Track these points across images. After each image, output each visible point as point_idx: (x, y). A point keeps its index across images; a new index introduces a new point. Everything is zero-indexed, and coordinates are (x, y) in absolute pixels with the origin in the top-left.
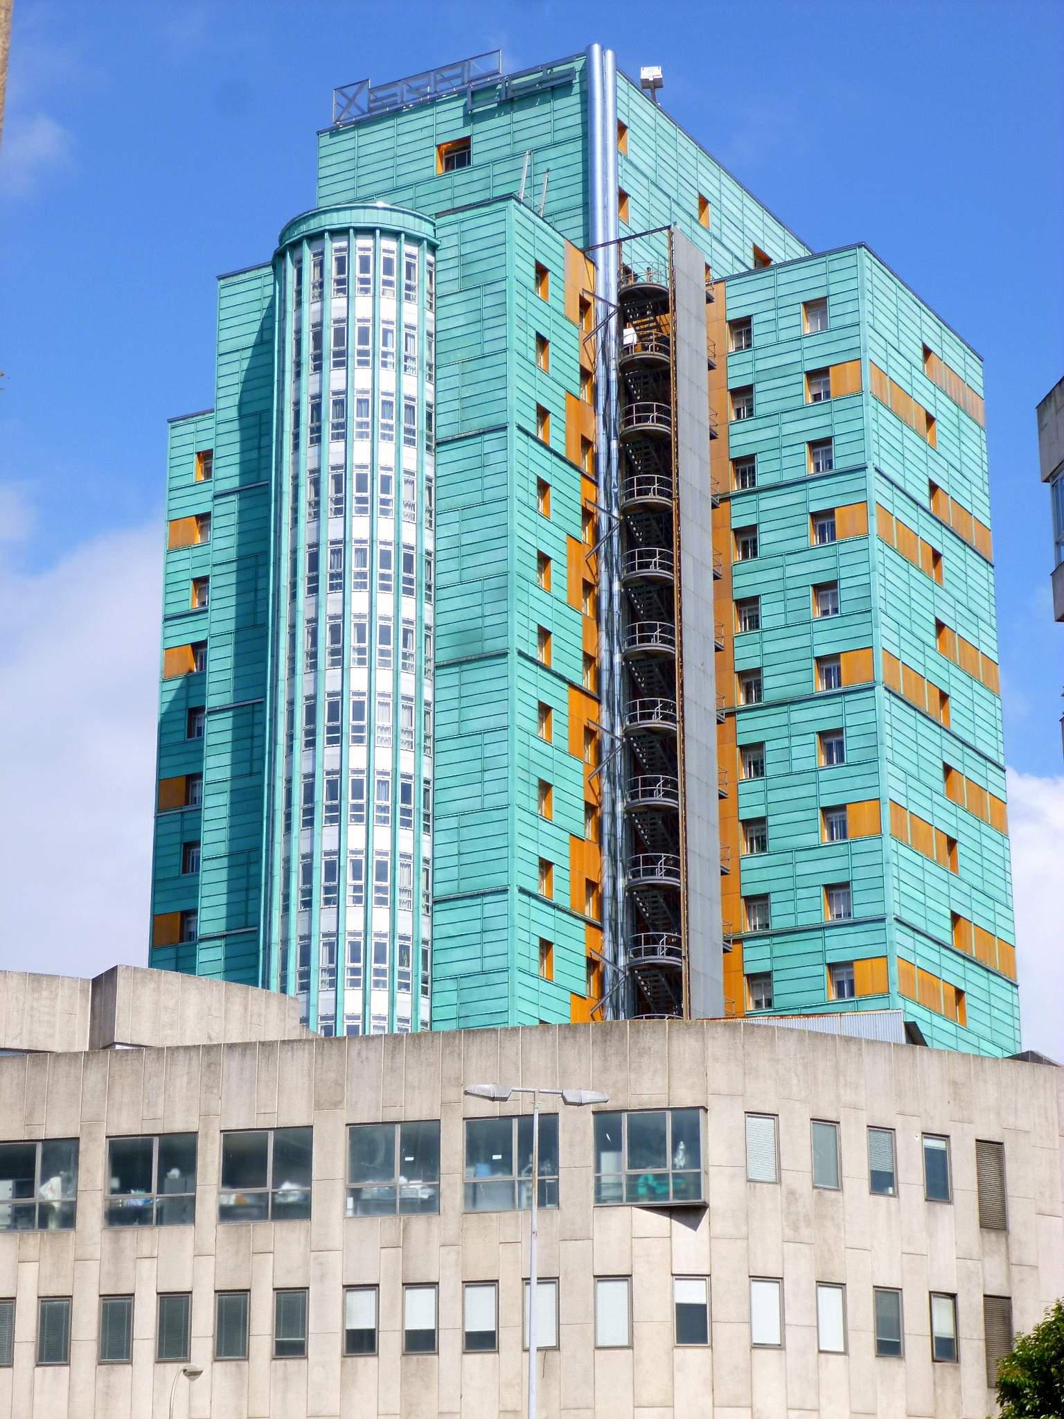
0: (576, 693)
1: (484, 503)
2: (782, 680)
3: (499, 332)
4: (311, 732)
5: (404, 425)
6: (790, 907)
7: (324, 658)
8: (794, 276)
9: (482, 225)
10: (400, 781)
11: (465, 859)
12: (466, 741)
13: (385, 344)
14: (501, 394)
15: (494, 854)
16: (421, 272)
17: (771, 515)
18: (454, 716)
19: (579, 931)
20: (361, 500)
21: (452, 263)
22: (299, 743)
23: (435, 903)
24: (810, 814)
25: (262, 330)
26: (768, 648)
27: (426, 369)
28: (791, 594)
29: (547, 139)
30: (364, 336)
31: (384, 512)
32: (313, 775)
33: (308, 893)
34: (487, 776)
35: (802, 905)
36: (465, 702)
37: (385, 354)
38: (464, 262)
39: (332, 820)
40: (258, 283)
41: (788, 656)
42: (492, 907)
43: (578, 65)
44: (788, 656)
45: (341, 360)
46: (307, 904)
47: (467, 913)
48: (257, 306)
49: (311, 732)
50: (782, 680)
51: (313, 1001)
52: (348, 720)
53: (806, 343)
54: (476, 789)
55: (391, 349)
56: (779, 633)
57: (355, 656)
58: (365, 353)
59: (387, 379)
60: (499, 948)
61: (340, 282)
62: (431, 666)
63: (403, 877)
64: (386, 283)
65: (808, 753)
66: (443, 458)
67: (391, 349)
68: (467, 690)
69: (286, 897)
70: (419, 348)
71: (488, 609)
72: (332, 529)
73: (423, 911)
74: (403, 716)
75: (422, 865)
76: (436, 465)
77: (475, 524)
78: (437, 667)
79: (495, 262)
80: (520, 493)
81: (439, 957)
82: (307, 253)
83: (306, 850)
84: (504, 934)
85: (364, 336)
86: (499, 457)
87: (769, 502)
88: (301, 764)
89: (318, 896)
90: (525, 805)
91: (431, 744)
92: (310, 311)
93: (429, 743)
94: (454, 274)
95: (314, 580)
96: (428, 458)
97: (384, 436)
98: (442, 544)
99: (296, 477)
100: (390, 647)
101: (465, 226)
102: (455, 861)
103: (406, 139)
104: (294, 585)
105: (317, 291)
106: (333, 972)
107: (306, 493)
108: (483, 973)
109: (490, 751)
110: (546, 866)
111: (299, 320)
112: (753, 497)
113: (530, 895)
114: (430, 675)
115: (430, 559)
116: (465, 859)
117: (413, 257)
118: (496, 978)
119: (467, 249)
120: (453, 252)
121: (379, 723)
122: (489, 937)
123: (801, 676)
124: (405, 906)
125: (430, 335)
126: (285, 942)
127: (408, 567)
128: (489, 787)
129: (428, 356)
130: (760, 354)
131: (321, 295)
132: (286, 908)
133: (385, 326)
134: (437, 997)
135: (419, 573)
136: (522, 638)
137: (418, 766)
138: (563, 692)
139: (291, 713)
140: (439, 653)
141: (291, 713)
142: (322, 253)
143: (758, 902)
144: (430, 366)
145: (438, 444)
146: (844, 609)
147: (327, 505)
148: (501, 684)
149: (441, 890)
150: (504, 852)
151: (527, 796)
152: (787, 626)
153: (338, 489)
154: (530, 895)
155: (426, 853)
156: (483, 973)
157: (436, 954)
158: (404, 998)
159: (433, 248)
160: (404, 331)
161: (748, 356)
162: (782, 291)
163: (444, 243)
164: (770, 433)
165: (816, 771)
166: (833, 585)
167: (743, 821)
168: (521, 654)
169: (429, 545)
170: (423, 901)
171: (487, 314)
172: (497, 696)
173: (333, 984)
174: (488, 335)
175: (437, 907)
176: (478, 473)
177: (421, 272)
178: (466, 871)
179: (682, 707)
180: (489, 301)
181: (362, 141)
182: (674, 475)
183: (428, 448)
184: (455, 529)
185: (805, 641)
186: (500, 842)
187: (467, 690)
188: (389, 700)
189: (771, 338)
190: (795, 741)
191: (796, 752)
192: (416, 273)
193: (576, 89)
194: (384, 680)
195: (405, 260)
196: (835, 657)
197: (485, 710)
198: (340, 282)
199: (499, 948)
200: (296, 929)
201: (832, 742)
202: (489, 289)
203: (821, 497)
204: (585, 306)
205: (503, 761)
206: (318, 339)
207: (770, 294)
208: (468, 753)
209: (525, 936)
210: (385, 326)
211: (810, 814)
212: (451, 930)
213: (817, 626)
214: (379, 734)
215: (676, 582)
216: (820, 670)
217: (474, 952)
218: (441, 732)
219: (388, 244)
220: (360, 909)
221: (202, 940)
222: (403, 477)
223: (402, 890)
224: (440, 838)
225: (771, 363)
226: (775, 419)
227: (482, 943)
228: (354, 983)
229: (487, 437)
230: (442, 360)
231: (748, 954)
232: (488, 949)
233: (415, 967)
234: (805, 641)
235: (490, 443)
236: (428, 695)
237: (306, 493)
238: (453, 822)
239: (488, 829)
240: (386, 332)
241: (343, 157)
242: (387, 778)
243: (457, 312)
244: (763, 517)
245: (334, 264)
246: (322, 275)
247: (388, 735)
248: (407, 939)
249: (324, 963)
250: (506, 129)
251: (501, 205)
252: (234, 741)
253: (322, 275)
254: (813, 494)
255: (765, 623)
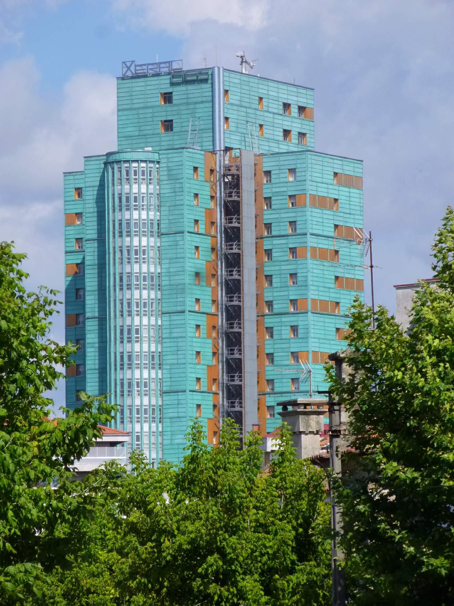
0: (209, 316)
1: (177, 258)
2: (279, 306)
3: (181, 198)
4: (122, 338)
5: (151, 362)
6: (278, 228)
7: (125, 313)
8: (285, 158)
9: (175, 157)
10: (151, 354)
11: (173, 379)
12: (172, 340)
13: (143, 202)
14: (182, 220)
15: (181, 379)
16: (155, 174)
17: (277, 246)
18: (168, 331)
19: (210, 397)
20: (135, 179)
21: (165, 169)
22: (118, 342)
23: (163, 393)
24: (287, 354)
25: (100, 181)
26: (275, 294)
27: (157, 207)
28: (283, 276)
29: (200, 99)
30: (136, 199)
31: (144, 262)
32: (123, 353)
33: (122, 391)
34: (179, 353)
35: (284, 384)
36: (172, 326)
37: (143, 205)
38: (169, 169)
39: (130, 368)
40: (98, 162)
41: (280, 298)
42: (181, 396)
43: (210, 72)
44: (280, 298)
45: (129, 234)
46: (122, 395)
47: (174, 397)
48: (98, 171)
49: (122, 338)
50: (279, 306)
51: (125, 427)
52: (134, 335)
53: (289, 184)
54: (175, 357)
55: (145, 203)
56: (278, 289)
57: (136, 313)
58: (137, 258)
59: (144, 215)
60: (183, 410)
61: (127, 206)
62: (160, 313)
63: (153, 386)
64: (143, 179)
65: (287, 333)
66: (163, 240)
67: (145, 203)
68: (173, 323)
69: (116, 392)
70: (154, 201)
71: (179, 296)
72: (127, 269)
73: (159, 396)
74: (152, 331)
75: (159, 381)
76: (161, 242)
77: (174, 265)
78: (162, 313)
79: (179, 172)
80: (189, 255)
81: (164, 358)
82: (116, 166)
83: (121, 324)
84: (185, 406)
85: (136, 199)
86: (181, 243)
87: (276, 241)
88: (119, 322)
89: (126, 393)
90: (191, 362)
91: (160, 340)
92: (117, 188)
93: (160, 339)
94: (165, 173)
95: (121, 286)
96: (158, 240)
97: (143, 235)
98: (163, 271)
99: (114, 248)
100: (147, 309)
101: (169, 156)
102: (169, 380)
103: (149, 88)
104: (115, 286)
105: (119, 181)
106: (131, 418)
107: (118, 255)
108: (178, 417)
109: (180, 397)
110: (198, 379)
111: (114, 190)
112: (271, 239)
113: (191, 233)
114: (160, 316)
115: (161, 355)
116: (173, 379)
117: (152, 168)
118: (183, 419)
119: (170, 165)
120: (165, 165)
121: (144, 335)
122: (180, 406)
123: (285, 306)
124: (153, 395)
125: (158, 195)
126: (115, 274)
127: (152, 281)
128: (180, 357)
129: (157, 203)
130: (274, 186)
131: (121, 183)
132: (116, 396)
133: (142, 195)
134: (164, 424)
135: (156, 281)
136: (189, 226)
137: (157, 349)
138: (204, 318)
139: (114, 198)
140: (163, 309)
141: (114, 198)
142: (121, 168)
143: (268, 226)
144: (158, 206)
145: (161, 235)
146: (299, 284)
147: (125, 260)
148: (183, 322)
149: (165, 389)
150: (184, 379)
151: (191, 357)
152: (281, 287)
153: (129, 254)
154: (191, 233)
155: (160, 376)
156: (178, 417)
157: (164, 357)
158: (154, 425)
159: (158, 162)
160: (149, 196)
161: (269, 186)
162: (282, 163)
163: (162, 161)
164: (277, 216)
165: (289, 339)
166: (296, 274)
167: (264, 172)
168: (188, 232)
169: (159, 270)
170: (159, 392)
171: (177, 190)
172: (181, 326)
173: (131, 422)
174: (177, 198)
175: (164, 395)
176: (175, 247)
177: (155, 174)
178: (173, 383)
179: (243, 323)
180: (177, 186)
181: (134, 85)
182: (243, 399)
183: (158, 236)
184: (167, 266)
185: (286, 293)
186: (183, 375)
187: (173, 323)
188: (147, 327)
189: (278, 181)
190: (283, 328)
191: (283, 332)
192: (152, 174)
193: (210, 81)
194: (145, 321)
195: (149, 169)
196: (296, 300)
197: (178, 330)
198: (129, 364)
199: (183, 410)
200: (118, 244)
201: (294, 329)
202: (178, 181)
203: (292, 242)
204: (212, 171)
205: (184, 348)
206: (120, 199)
207: (277, 163)
208: (173, 344)
209: (191, 352)
210: (142, 195)
211: (287, 354)
212: (168, 402)
213: (290, 288)
214: (144, 339)
215: (243, 412)
216: (290, 252)
217: (176, 410)
218: (164, 336)
219: (143, 165)
220: (139, 317)
221: (88, 319)
222: (150, 248)
223: (153, 444)
224: (165, 371)
225: (277, 190)
226: (278, 212)
227: (178, 408)
228: (138, 422)
229: (177, 235)
230: (162, 204)
231: (265, 243)
232: (180, 410)
233: (157, 414)
234: (286, 293)
235: (178, 237)
236: (159, 323)
237: (118, 255)
238: (168, 367)
239: (180, 371)
240: (143, 197)
241: (126, 90)
242: (146, 354)
243: (166, 190)
244: (275, 247)
245: (125, 172)
246: (121, 176)
247: (147, 339)
248: (154, 406)
249: (128, 415)
250: (185, 92)
251: (181, 150)
252: (97, 199)
253: (121, 176)
254: (290, 241)
255: (274, 285)
